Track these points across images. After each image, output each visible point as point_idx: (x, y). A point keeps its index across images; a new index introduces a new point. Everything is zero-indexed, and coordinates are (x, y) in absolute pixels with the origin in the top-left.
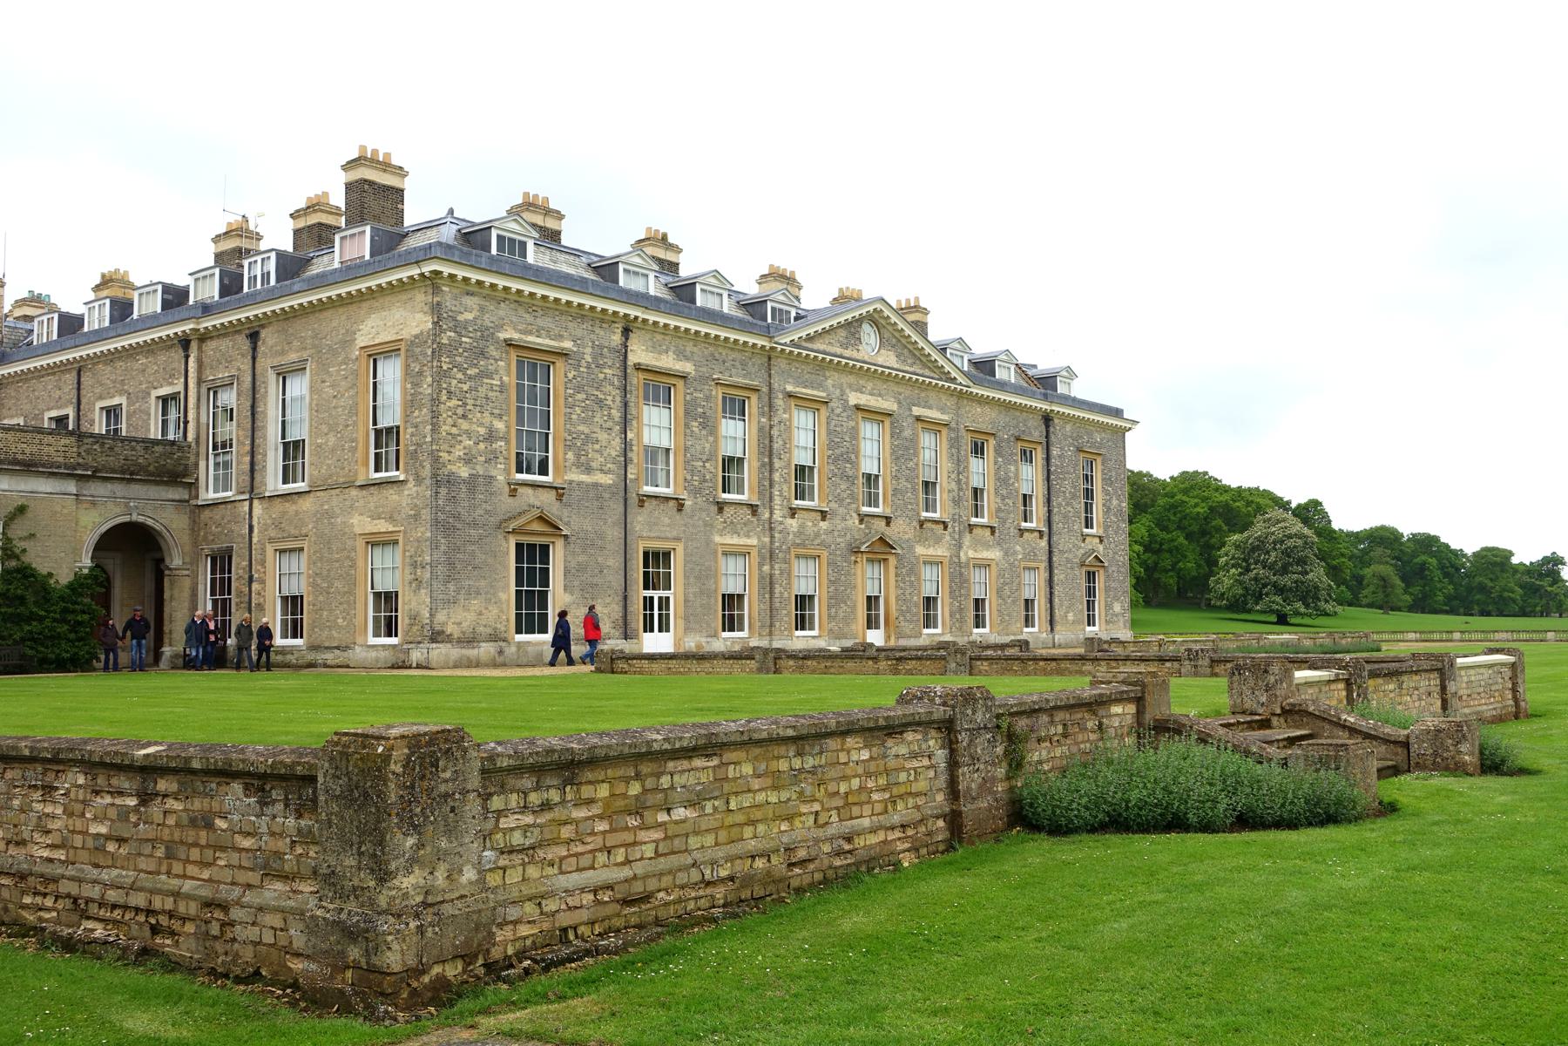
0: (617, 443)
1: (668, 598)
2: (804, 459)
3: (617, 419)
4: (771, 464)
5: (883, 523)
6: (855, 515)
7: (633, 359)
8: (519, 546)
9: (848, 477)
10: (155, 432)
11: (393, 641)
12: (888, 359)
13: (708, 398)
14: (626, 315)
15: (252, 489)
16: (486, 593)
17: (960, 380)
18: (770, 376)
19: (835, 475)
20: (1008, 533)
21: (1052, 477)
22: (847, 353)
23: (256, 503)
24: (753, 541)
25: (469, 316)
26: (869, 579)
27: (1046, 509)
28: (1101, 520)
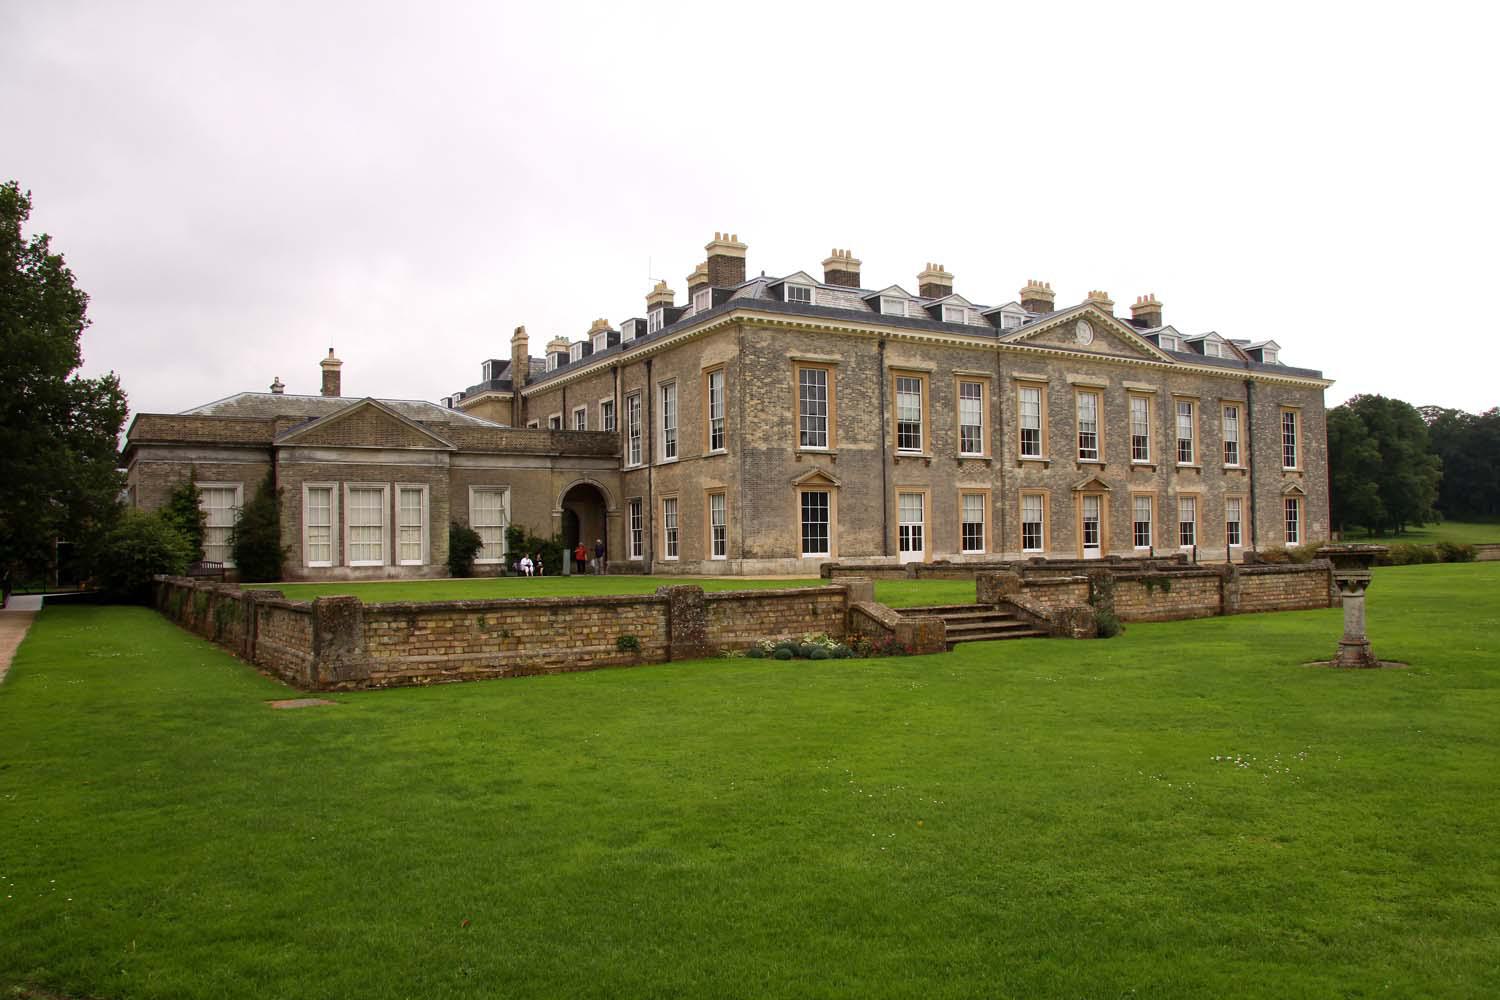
0: (876, 421)
1: (920, 528)
2: (1031, 425)
3: (877, 405)
4: (1001, 429)
5: (1099, 468)
6: (1074, 464)
7: (887, 362)
8: (804, 495)
9: (1067, 436)
10: (602, 428)
11: (724, 557)
12: (1102, 347)
13: (948, 386)
14: (880, 334)
15: (650, 458)
16: (782, 526)
17: (1164, 358)
18: (999, 367)
19: (1056, 435)
20: (1213, 473)
21: (1253, 428)
22: (1064, 345)
23: (653, 470)
24: (988, 485)
25: (764, 344)
26: (1086, 509)
27: (1248, 453)
28: (1301, 459)
